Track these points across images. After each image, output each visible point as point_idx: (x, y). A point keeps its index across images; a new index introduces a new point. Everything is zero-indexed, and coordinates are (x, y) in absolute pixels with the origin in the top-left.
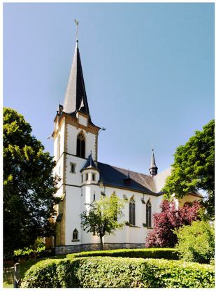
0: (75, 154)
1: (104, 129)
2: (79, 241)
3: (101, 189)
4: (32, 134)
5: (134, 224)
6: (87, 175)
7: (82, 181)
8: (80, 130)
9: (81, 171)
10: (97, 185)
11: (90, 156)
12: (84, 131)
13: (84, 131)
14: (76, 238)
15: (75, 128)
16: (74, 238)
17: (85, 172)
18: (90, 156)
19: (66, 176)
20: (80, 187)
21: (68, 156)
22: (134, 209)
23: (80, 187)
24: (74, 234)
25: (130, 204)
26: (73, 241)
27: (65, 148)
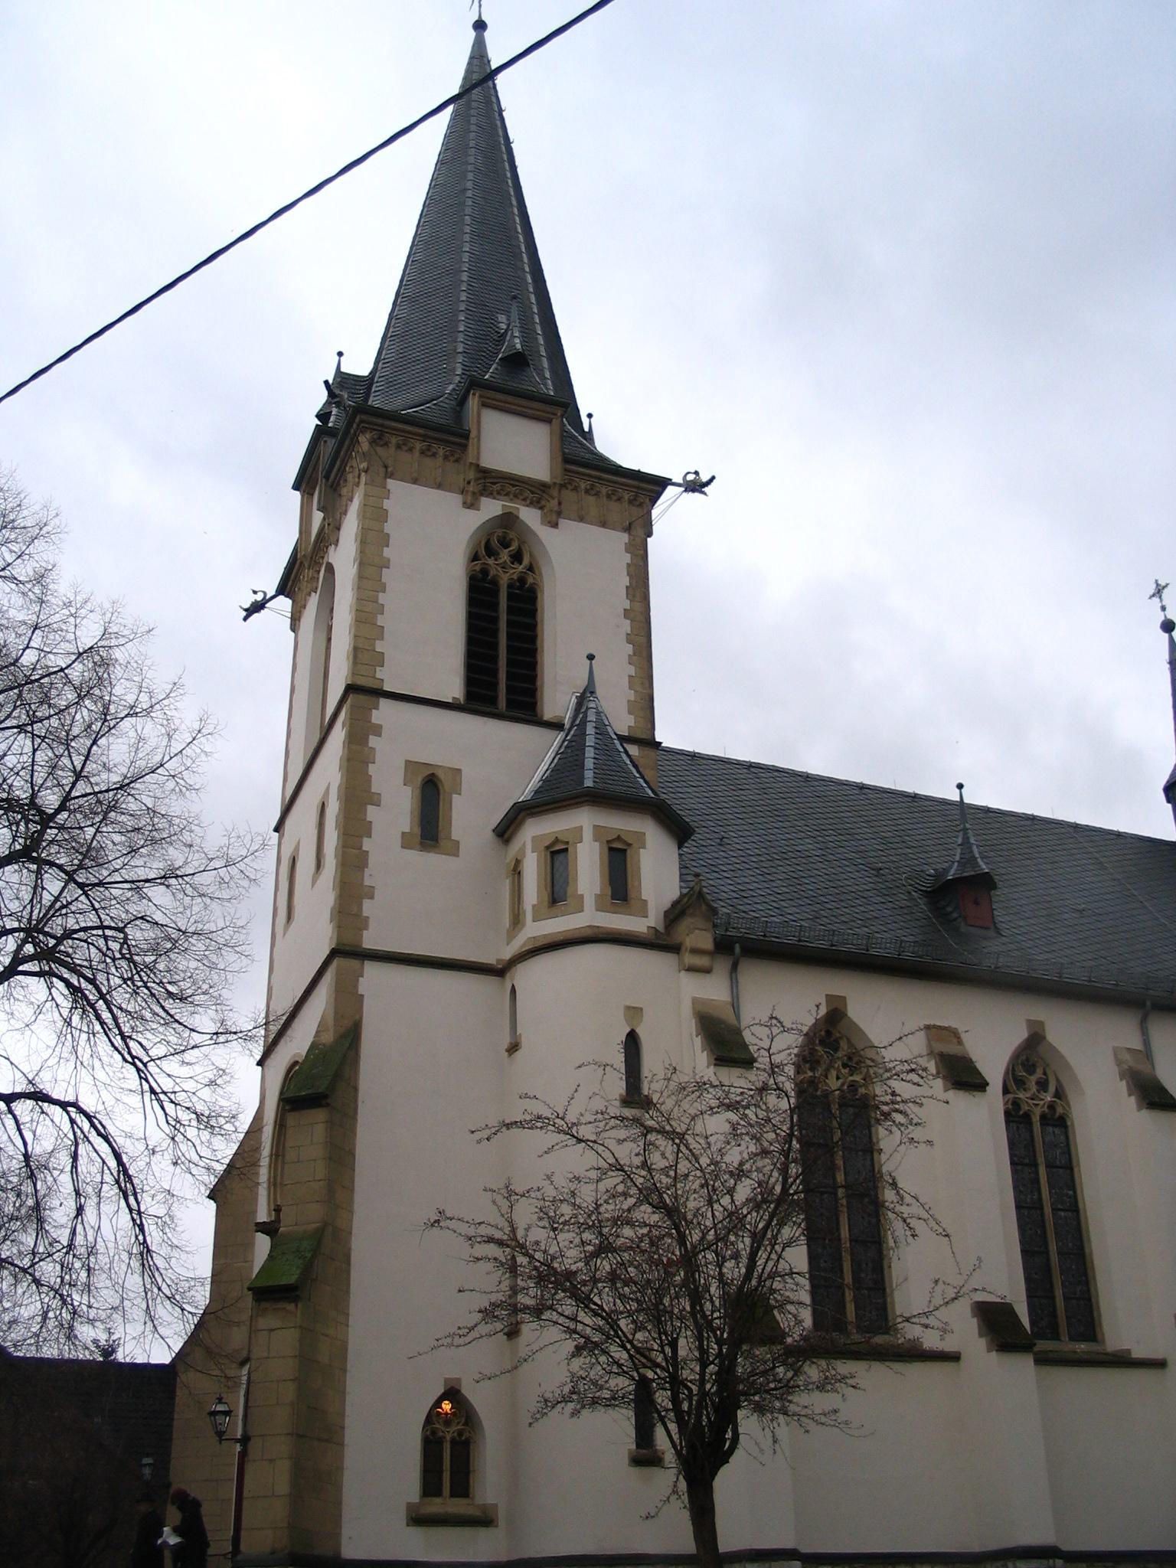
0: (453, 688)
1: (696, 486)
2: (484, 1520)
3: (1000, 884)
4: (649, 539)
5: (1086, 1323)
6: (557, 853)
7: (517, 921)
8: (492, 508)
9: (506, 830)
10: (661, 942)
11: (588, 693)
12: (529, 516)
13: (529, 516)
14: (462, 1488)
15: (453, 500)
16: (430, 1486)
17: (536, 831)
18: (588, 693)
19: (372, 876)
20: (499, 971)
21: (385, 712)
22: (1065, 1168)
23: (499, 971)
24: (431, 1444)
25: (1015, 1117)
26: (418, 1519)
27: (364, 653)
